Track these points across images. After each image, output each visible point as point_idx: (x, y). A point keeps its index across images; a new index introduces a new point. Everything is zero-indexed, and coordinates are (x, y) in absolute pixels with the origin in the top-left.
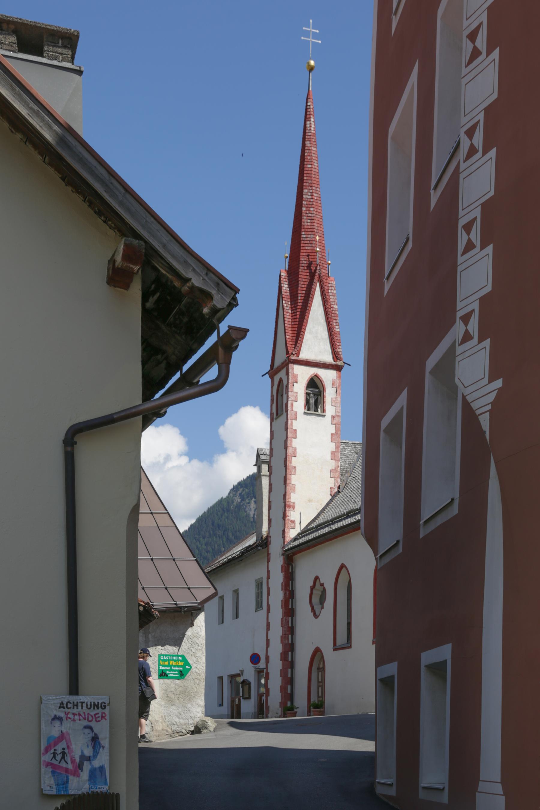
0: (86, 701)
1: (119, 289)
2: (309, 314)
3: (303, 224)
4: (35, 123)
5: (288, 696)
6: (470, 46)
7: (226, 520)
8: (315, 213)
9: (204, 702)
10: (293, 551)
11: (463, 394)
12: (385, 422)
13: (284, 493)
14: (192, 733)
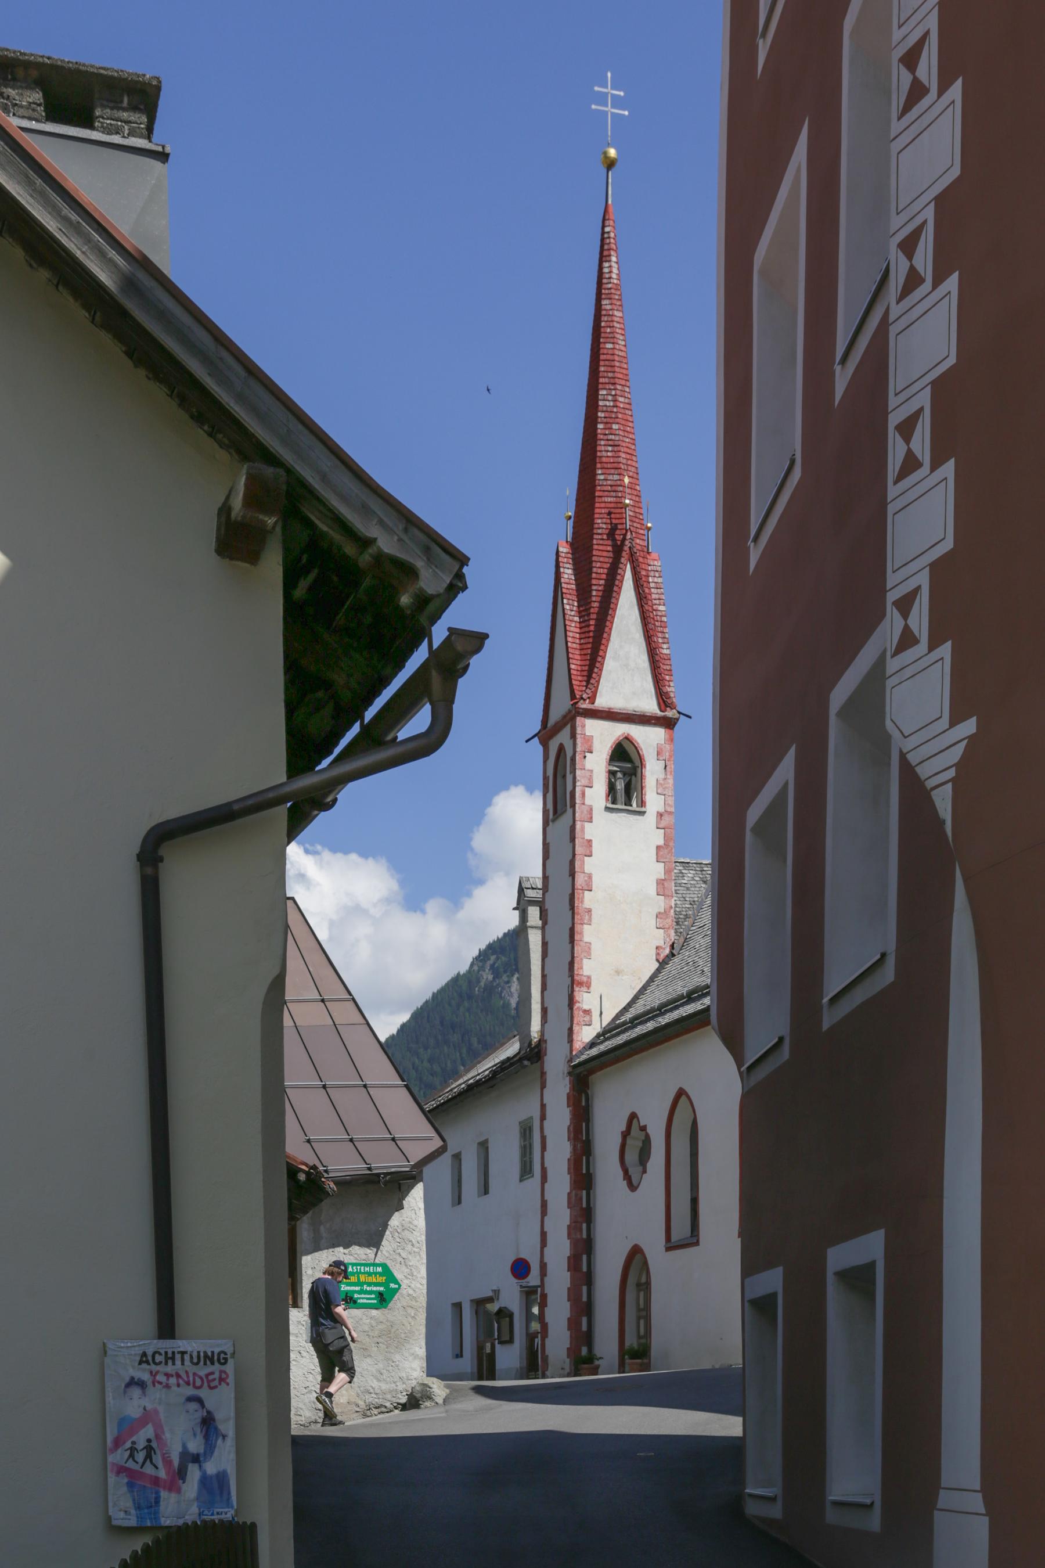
0: (189, 1349)
1: (239, 563)
2: (612, 623)
3: (599, 454)
4: (73, 246)
5: (583, 1337)
6: (906, 78)
7: (467, 1014)
8: (621, 433)
9: (424, 1350)
10: (588, 1066)
11: (901, 751)
12: (754, 813)
14: (404, 1407)
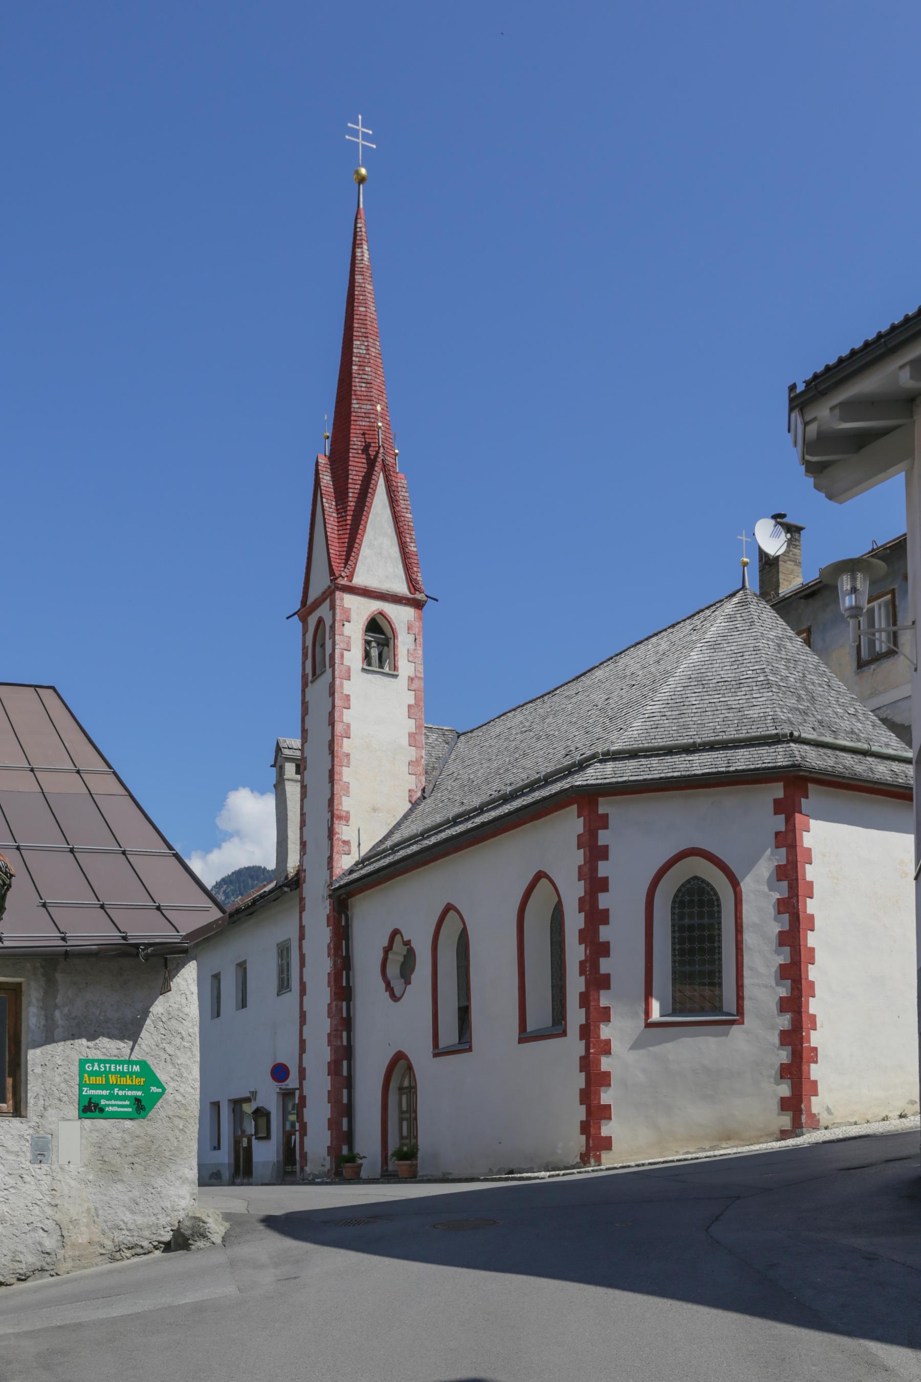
2: (367, 518)
3: (354, 388)
9: (196, 1171)
10: (348, 888)
13: (329, 796)
14: (168, 1247)
